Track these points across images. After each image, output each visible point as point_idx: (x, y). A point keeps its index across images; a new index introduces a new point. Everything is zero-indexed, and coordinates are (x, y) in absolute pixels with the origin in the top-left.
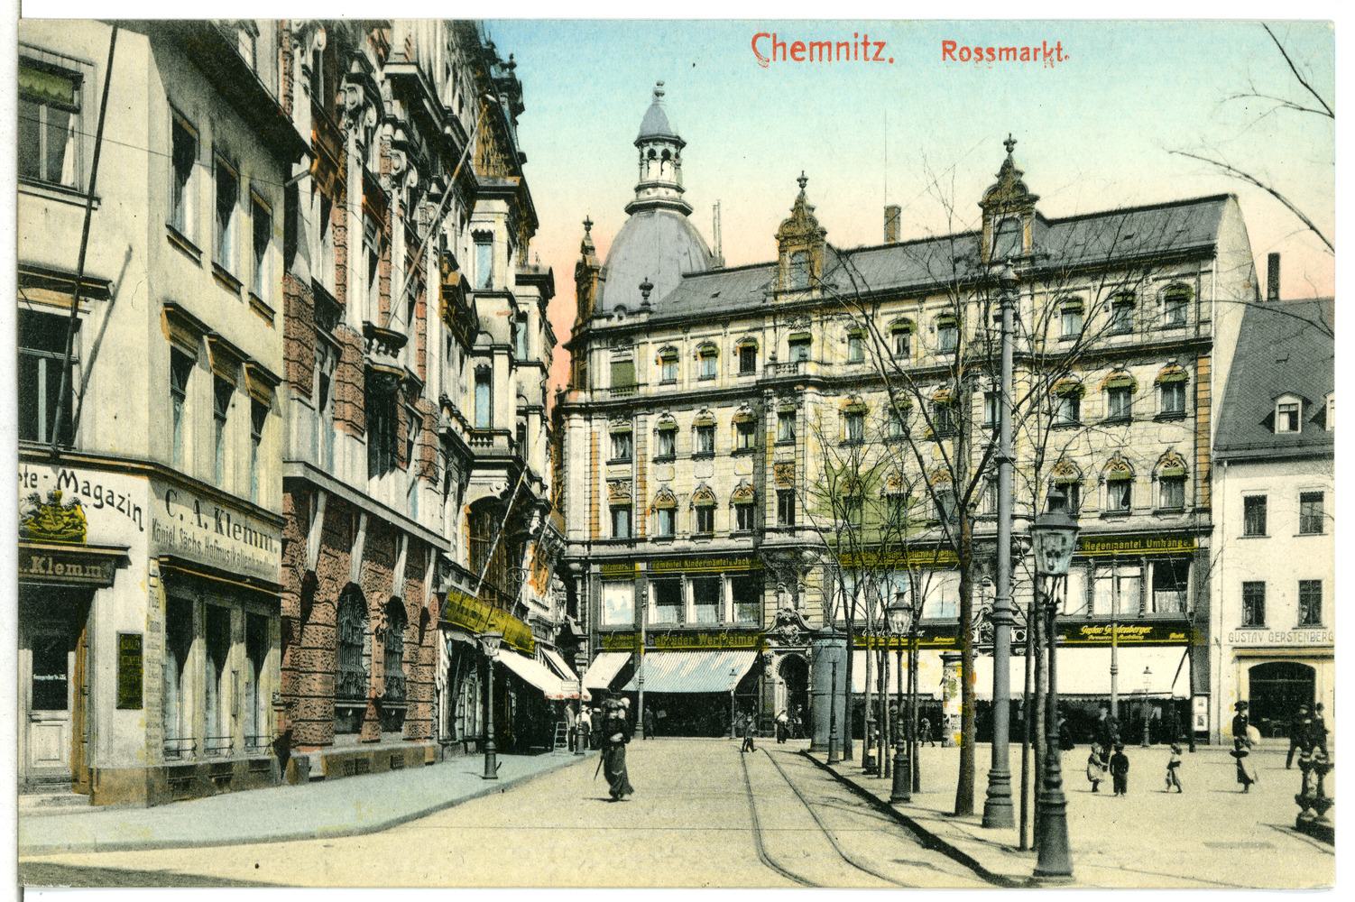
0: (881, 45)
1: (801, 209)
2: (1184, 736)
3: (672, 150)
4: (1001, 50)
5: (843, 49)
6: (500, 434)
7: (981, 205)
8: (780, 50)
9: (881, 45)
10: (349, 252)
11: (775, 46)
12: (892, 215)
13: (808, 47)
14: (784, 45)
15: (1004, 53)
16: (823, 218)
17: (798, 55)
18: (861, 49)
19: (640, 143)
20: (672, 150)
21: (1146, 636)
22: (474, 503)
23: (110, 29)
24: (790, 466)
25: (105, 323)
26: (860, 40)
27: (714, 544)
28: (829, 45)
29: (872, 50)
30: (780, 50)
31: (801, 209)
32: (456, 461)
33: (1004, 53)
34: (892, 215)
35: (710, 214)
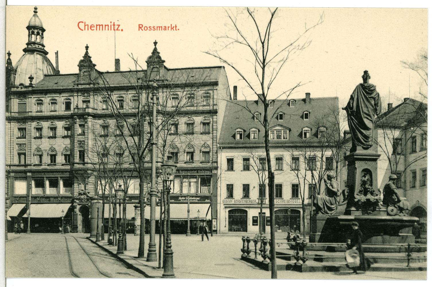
4: (97, 25)
8: (86, 27)
13: (95, 26)
17: (92, 28)
20: (40, 32)
26: (112, 24)
30: (86, 27)
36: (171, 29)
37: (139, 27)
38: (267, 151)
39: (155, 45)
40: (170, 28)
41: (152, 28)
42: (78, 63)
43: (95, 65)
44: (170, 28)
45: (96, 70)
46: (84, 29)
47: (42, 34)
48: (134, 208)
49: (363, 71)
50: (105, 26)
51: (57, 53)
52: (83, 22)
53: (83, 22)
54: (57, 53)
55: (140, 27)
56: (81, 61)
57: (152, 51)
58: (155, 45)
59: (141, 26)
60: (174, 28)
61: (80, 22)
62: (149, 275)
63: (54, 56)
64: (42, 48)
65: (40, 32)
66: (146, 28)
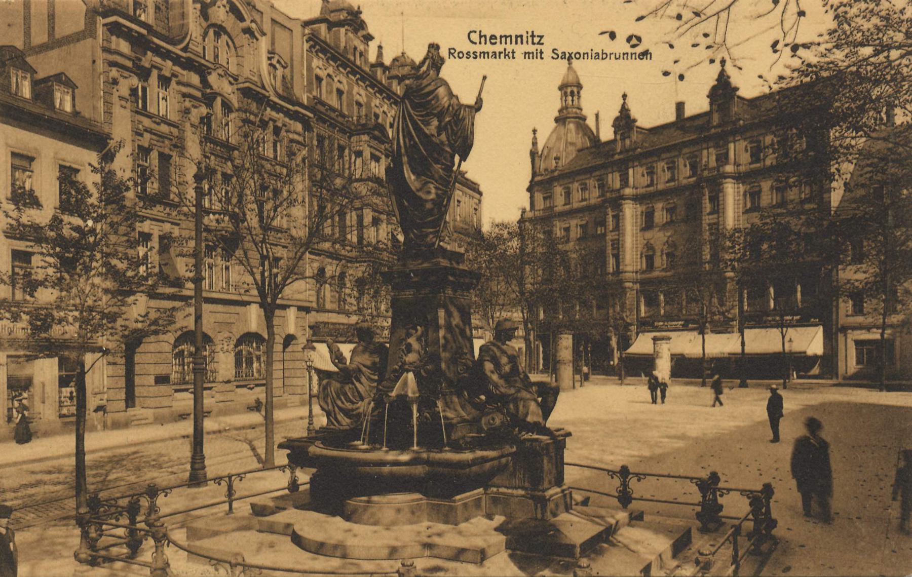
0: (541, 37)
1: (625, 111)
3: (575, 90)
4: (501, 37)
5: (519, 39)
7: (708, 96)
8: (483, 39)
9: (541, 37)
10: (10, 182)
12: (680, 106)
13: (498, 38)
14: (485, 36)
15: (503, 39)
16: (634, 113)
17: (493, 41)
18: (530, 39)
19: (560, 88)
24: (715, 226)
26: (530, 34)
27: (656, 274)
28: (511, 36)
29: (536, 40)
30: (483, 39)
31: (625, 111)
32: (515, 282)
33: (503, 39)
34: (680, 106)
35: (594, 119)
36: (505, 56)
37: (450, 53)
38: (884, 322)
40: (502, 55)
41: (472, 55)
43: (737, 89)
44: (502, 55)
45: (739, 97)
46: (478, 41)
49: (525, 190)
50: (517, 37)
52: (475, 32)
53: (475, 32)
57: (716, 77)
59: (452, 51)
60: (511, 55)
61: (471, 32)
62: (780, 428)
66: (461, 55)
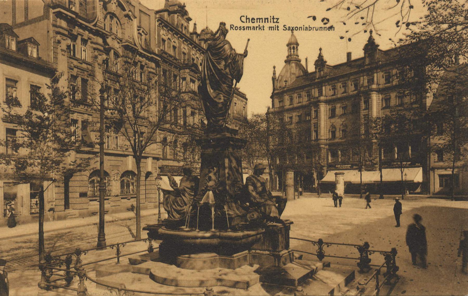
0: (278, 19)
1: (320, 57)
2: (262, 208)
4: (257, 19)
5: (266, 20)
6: (100, 205)
7: (363, 49)
8: (248, 20)
9: (278, 19)
11: (247, 19)
12: (349, 55)
13: (256, 19)
14: (249, 19)
15: (258, 20)
16: (326, 58)
17: (253, 21)
19: (288, 45)
20: (295, 46)
21: (409, 165)
22: (300, 279)
23: (30, 17)
25: (143, 292)
26: (272, 17)
28: (262, 19)
29: (275, 20)
30: (248, 20)
31: (320, 57)
33: (258, 20)
34: (349, 55)
36: (259, 29)
37: (231, 27)
38: (454, 165)
39: (320, 51)
40: (258, 28)
41: (242, 28)
42: (314, 63)
43: (378, 46)
44: (258, 28)
45: (379, 50)
46: (245, 21)
47: (297, 47)
48: (361, 243)
49: (269, 97)
50: (265, 19)
51: (306, 59)
52: (244, 16)
53: (244, 16)
54: (306, 59)
55: (249, 40)
56: (316, 61)
57: (367, 39)
58: (320, 51)
59: (232, 26)
60: (262, 28)
61: (242, 16)
63: (305, 61)
64: (297, 57)
65: (295, 46)
66: (236, 28)
